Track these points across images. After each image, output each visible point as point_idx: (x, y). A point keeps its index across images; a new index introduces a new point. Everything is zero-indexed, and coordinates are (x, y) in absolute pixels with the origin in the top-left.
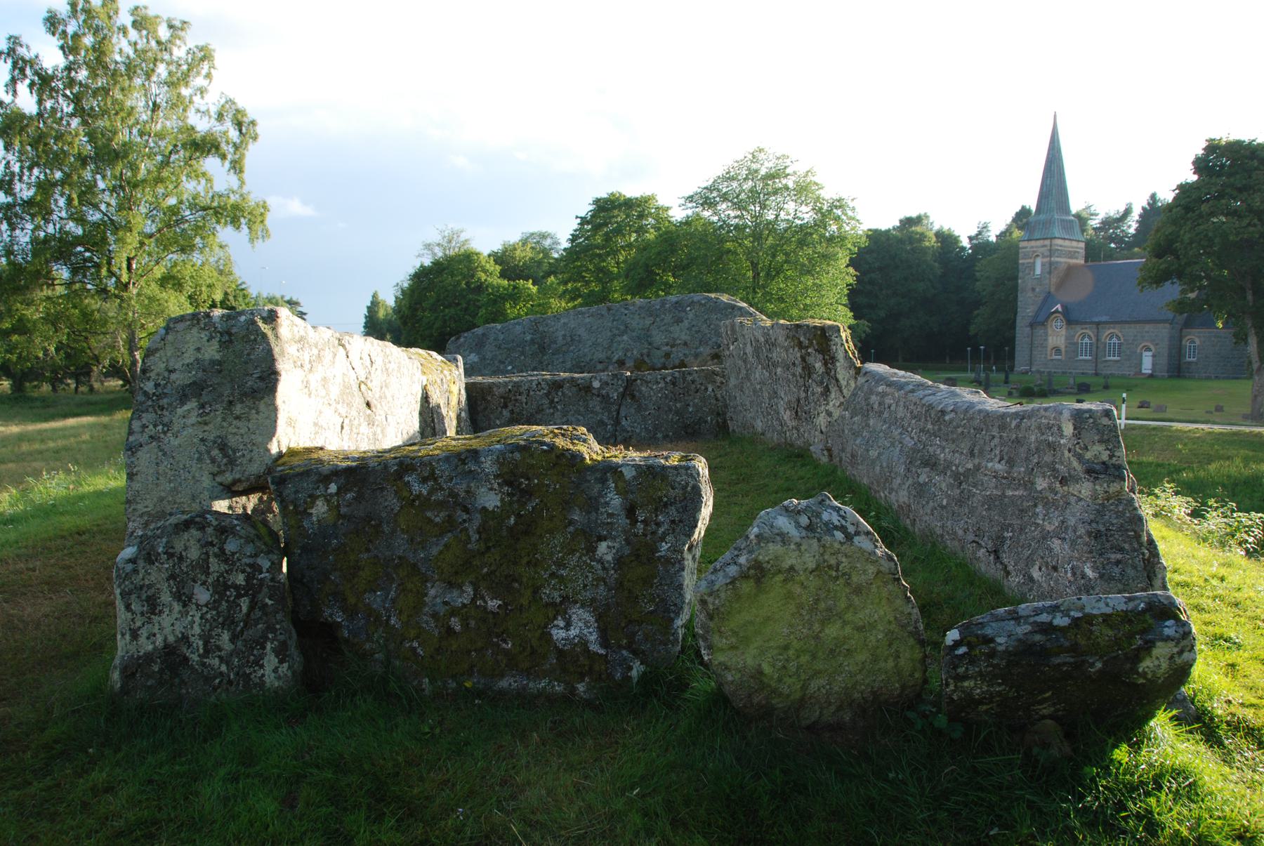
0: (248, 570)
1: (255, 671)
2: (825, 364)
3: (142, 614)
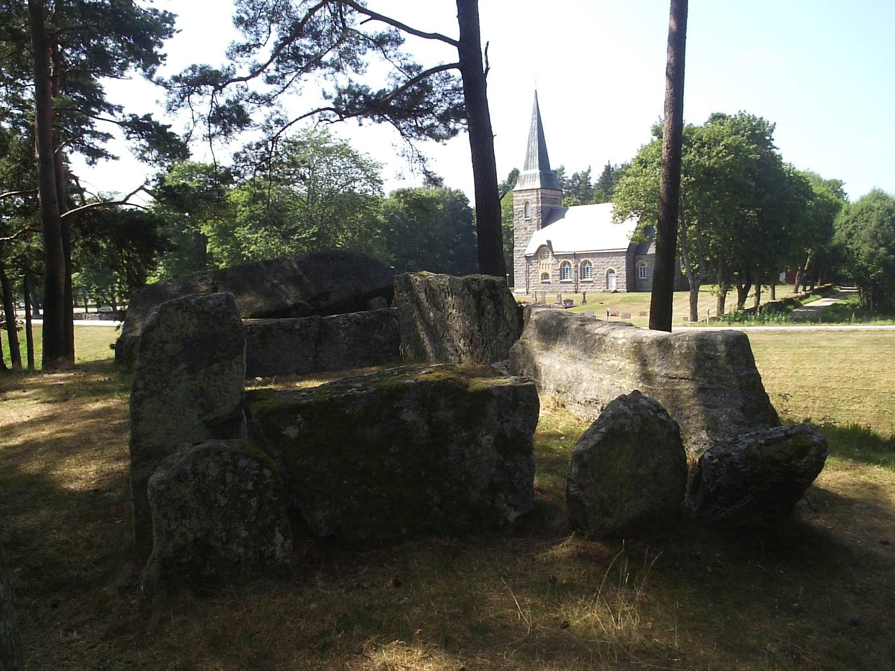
0: (255, 478)
1: (268, 548)
2: (495, 306)
3: (176, 519)
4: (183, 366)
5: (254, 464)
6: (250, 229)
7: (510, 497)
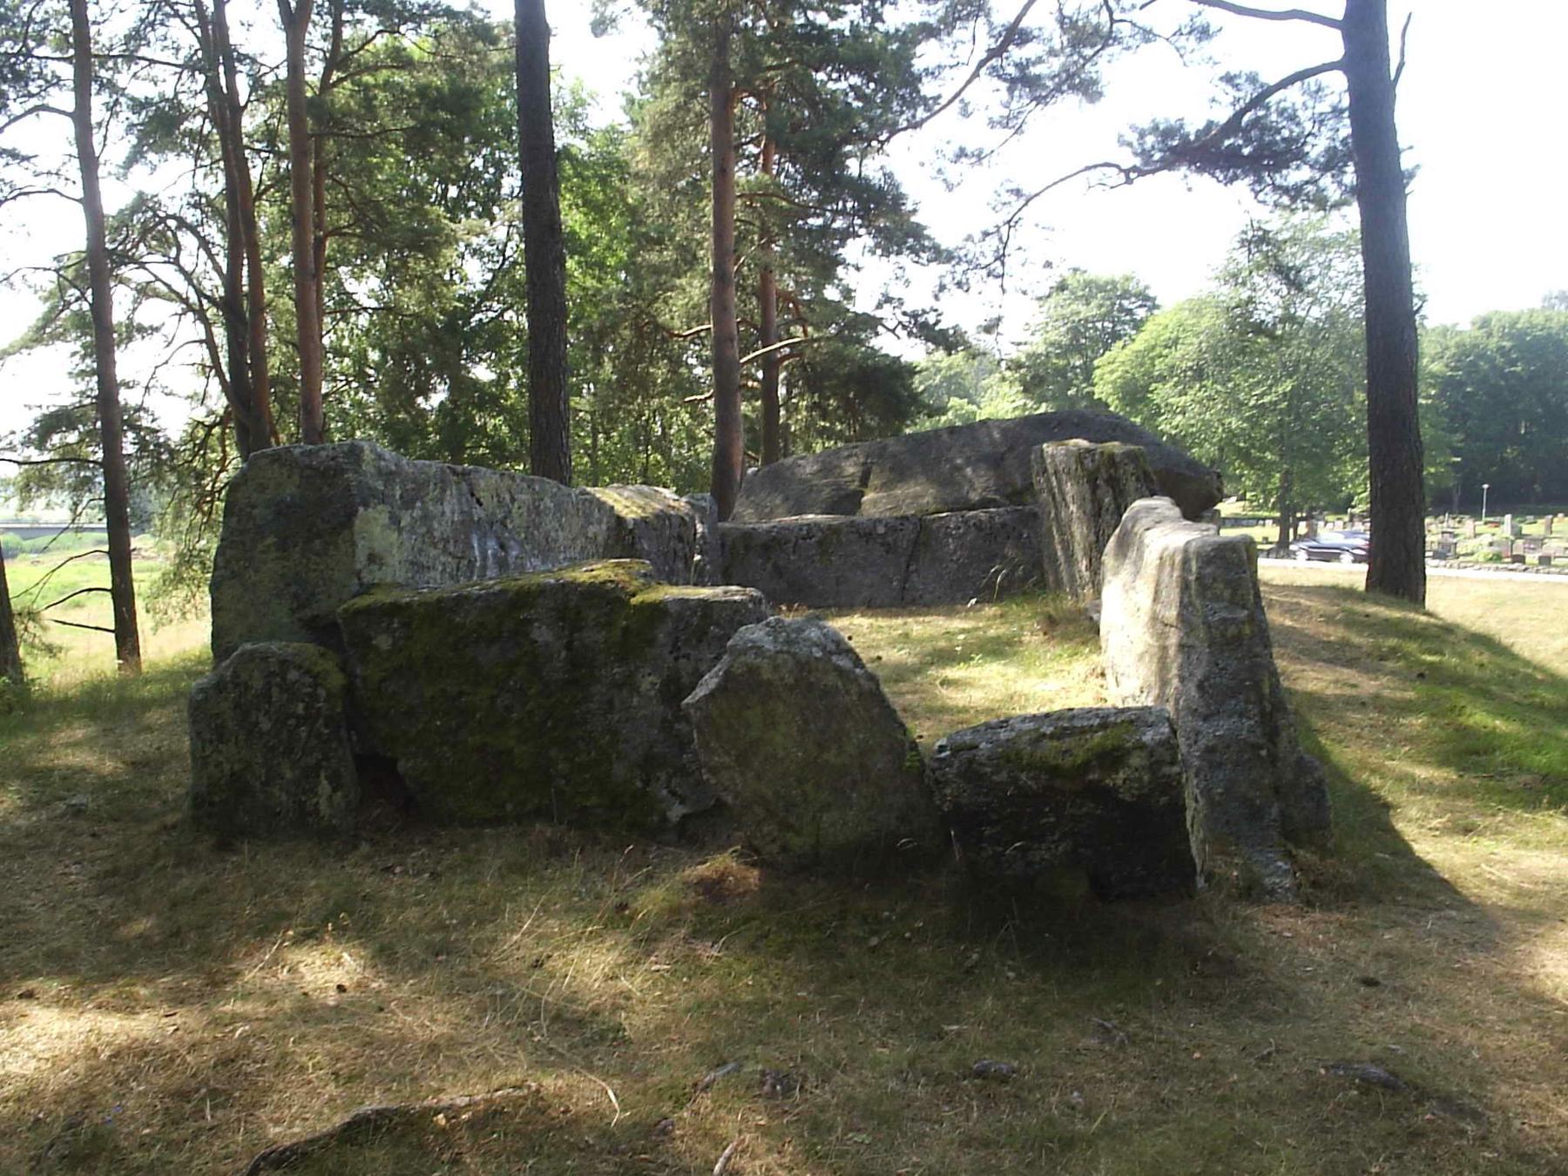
2: (1115, 499)
4: (271, 540)
5: (308, 680)
6: (1176, 385)
7: (674, 781)
